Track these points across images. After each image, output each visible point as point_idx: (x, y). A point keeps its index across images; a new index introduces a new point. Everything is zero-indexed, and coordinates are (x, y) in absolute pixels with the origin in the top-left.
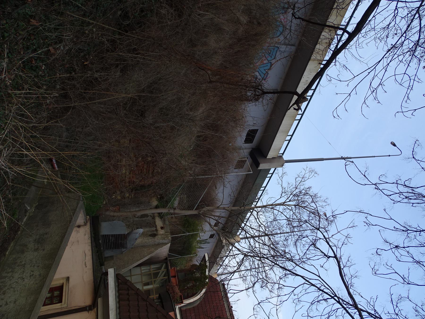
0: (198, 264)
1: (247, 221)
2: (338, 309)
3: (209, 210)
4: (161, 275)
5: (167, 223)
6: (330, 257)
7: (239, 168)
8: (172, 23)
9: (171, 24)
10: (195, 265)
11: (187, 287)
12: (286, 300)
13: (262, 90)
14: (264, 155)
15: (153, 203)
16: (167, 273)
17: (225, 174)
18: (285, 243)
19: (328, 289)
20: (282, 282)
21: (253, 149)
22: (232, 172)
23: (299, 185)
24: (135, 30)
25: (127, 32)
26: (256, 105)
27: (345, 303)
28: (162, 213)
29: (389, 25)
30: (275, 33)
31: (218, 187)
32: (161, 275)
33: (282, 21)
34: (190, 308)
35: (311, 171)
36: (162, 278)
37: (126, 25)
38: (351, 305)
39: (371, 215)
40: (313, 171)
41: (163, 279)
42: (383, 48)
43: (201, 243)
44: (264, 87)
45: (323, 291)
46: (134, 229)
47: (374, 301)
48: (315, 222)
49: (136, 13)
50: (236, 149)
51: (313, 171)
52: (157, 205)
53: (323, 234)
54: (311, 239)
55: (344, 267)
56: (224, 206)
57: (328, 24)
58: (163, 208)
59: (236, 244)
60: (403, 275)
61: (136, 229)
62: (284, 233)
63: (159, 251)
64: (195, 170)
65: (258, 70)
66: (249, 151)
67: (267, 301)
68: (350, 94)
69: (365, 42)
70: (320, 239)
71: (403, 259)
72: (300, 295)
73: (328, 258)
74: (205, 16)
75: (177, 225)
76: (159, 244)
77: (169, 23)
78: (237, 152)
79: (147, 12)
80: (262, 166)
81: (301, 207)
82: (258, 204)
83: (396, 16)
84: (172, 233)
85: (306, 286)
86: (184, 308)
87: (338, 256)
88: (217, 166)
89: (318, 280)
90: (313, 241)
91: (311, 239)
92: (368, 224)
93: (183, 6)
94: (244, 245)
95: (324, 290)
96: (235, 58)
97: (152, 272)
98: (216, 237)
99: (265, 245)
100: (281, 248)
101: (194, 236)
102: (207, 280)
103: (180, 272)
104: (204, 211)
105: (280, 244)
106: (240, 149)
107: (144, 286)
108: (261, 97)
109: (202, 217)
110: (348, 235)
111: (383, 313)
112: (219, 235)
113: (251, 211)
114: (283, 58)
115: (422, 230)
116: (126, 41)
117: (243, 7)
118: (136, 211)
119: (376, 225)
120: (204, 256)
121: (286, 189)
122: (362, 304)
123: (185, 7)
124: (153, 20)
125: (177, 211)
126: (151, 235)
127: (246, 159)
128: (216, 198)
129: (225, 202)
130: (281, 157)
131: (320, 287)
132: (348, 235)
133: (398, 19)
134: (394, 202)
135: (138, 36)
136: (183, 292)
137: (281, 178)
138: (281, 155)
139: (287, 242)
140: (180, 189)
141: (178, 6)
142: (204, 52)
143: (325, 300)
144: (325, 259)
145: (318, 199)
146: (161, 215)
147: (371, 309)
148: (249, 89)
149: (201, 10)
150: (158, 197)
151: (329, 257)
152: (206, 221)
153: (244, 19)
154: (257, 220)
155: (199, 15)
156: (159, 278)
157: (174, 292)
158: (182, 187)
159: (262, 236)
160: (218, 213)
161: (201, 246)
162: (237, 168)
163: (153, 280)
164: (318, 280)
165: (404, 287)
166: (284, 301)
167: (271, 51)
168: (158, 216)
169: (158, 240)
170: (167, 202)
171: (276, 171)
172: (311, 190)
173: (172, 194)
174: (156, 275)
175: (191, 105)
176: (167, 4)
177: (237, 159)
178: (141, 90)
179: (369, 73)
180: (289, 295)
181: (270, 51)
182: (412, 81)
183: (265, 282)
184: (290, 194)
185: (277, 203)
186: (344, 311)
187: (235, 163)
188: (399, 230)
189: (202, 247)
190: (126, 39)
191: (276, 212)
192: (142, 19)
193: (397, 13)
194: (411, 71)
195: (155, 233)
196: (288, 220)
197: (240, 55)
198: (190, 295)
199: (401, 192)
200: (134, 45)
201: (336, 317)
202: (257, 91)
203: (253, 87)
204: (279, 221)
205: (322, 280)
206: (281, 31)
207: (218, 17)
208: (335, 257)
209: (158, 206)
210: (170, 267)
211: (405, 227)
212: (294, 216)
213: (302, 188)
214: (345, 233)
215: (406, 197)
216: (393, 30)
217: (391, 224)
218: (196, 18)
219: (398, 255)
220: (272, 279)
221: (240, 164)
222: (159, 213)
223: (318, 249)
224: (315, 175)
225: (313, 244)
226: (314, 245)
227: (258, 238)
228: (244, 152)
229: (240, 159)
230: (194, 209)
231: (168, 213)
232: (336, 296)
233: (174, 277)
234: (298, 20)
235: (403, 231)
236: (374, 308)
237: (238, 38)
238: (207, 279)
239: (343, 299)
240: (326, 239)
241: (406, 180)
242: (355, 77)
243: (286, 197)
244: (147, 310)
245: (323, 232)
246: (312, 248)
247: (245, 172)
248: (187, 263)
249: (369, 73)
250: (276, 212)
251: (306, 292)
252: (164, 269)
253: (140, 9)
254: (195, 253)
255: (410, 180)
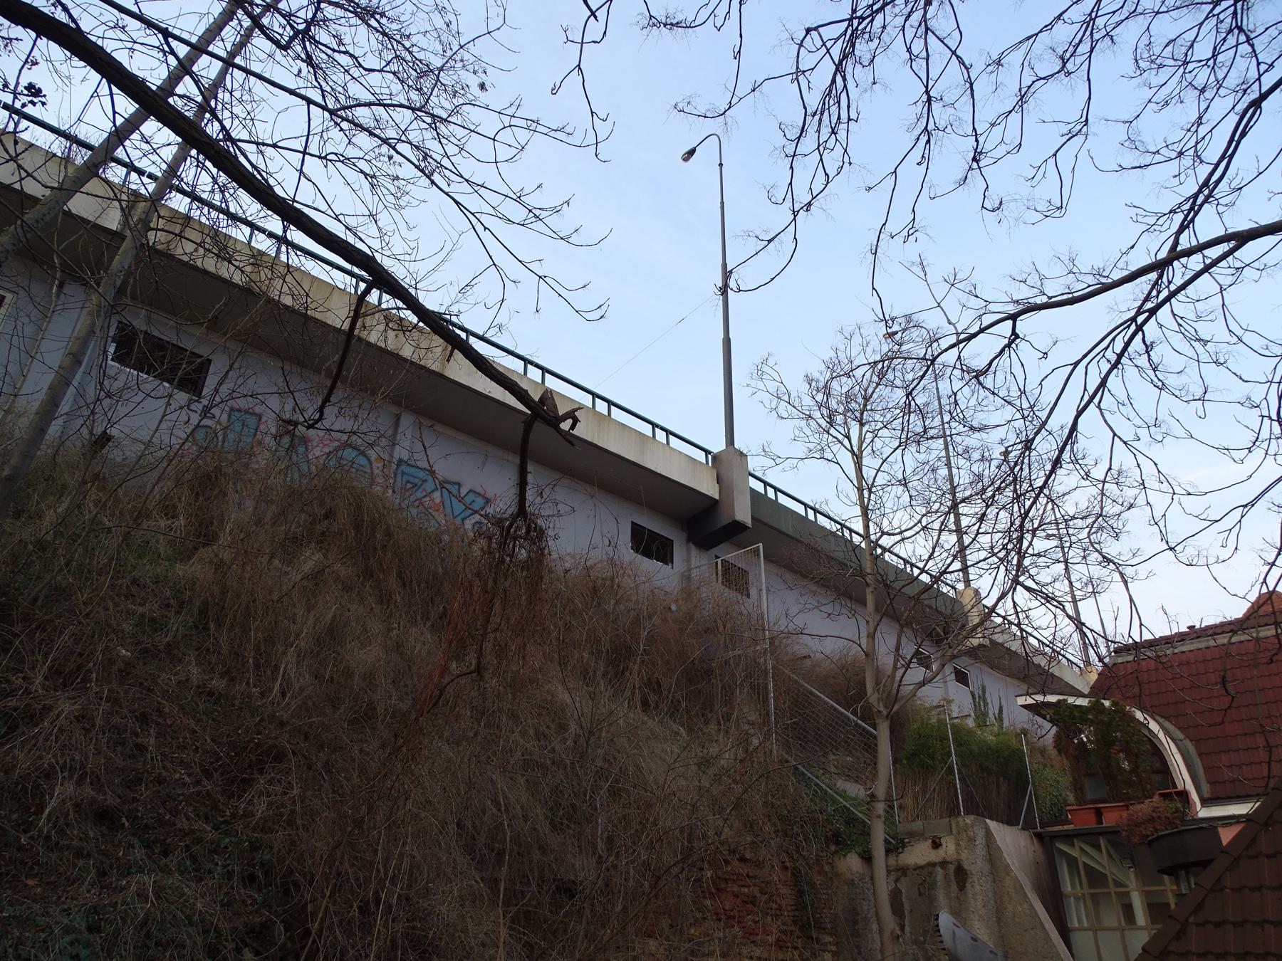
0: (1054, 729)
1: (912, 565)
2: (1174, 315)
3: (877, 684)
4: (1099, 863)
5: (918, 825)
6: (1014, 332)
7: (747, 583)
8: (297, 784)
9: (301, 787)
10: (1058, 738)
11: (1130, 772)
12: (1156, 464)
13: (514, 517)
14: (708, 507)
15: (854, 869)
16: (1090, 837)
17: (764, 630)
18: (976, 456)
19: (1114, 339)
20: (1098, 473)
21: (688, 540)
22: (760, 606)
23: (800, 409)
24: (306, 904)
25: (308, 933)
26: (556, 538)
27: (1154, 293)
28: (886, 841)
29: (366, 175)
30: (357, 470)
31: (804, 652)
32: (1099, 863)
33: (327, 450)
34: (1204, 768)
35: (759, 373)
36: (1104, 859)
37: (289, 934)
38: (1160, 277)
39: (885, 224)
40: (759, 367)
41: (1109, 855)
42: (420, 187)
43: (985, 715)
44: (504, 513)
45: (1120, 356)
46: (941, 946)
47: (1145, 213)
48: (911, 370)
49: (256, 900)
50: (689, 590)
51: (759, 367)
52: (859, 855)
53: (946, 350)
54: (961, 384)
55: (1044, 294)
56: (864, 633)
57: (346, 326)
58: (869, 835)
59: (989, 602)
60: (1063, 136)
61: (940, 936)
62: (948, 457)
63: (1015, 861)
64: (749, 723)
65: (459, 519)
66: (694, 551)
67: (1161, 524)
68: (540, 277)
69: (405, 233)
70: (959, 357)
71: (1012, 135)
72: (1139, 422)
73: (1017, 336)
74: (289, 678)
75: (925, 792)
76: (991, 860)
77: (295, 792)
78: (698, 588)
79: (255, 862)
80: (743, 513)
81: (865, 405)
82: (856, 530)
83: (343, 156)
84: (953, 812)
85: (1107, 401)
86: (1206, 788)
87: (1012, 309)
88: (740, 652)
89: (1086, 368)
90: (967, 377)
91: (961, 384)
92: (911, 230)
93: (252, 745)
94: (988, 584)
95: (1118, 352)
96: (419, 586)
97: (1087, 890)
98: (962, 663)
99: (984, 515)
100: (990, 471)
101: (962, 737)
102: (1107, 703)
103: (1082, 793)
104: (879, 699)
105: (981, 469)
106: (689, 578)
107: (1135, 924)
108: (533, 522)
109: (899, 709)
110: (945, 280)
111: (1178, 189)
112: (961, 654)
113: (879, 551)
114: (427, 456)
115: (925, 98)
116: (335, 937)
117: (276, 562)
118: (881, 931)
119: (913, 211)
120: (1024, 706)
121: (811, 446)
122: (1154, 247)
123: (255, 738)
124: (282, 843)
125: (881, 791)
126: (962, 884)
127: (719, 561)
128: (840, 659)
129: (850, 632)
130: (714, 458)
131: (1109, 361)
132: (945, 280)
133: (351, 152)
134: (846, 165)
135: (323, 897)
136: (1149, 786)
137: (778, 461)
138: (710, 456)
139: (975, 449)
140: (809, 775)
141: (251, 761)
142: (394, 682)
143: (1148, 348)
144: (1022, 346)
145: (842, 356)
146: (895, 846)
147: (1169, 221)
148: (508, 555)
149: (271, 690)
150: (836, 852)
151: (1015, 335)
152: (915, 695)
153: (311, 559)
154: (907, 534)
155: (284, 694)
156: (1104, 867)
157: (1151, 820)
158: (804, 767)
159: (957, 522)
160: (885, 657)
161: (994, 714)
162: (748, 590)
163: (1113, 889)
164: (1086, 368)
165: (1096, 135)
166: (1159, 471)
167: (408, 482)
168: (897, 856)
169: (975, 863)
170: (851, 821)
171: (759, 474)
172: (816, 375)
173: (826, 801)
174: (1095, 878)
175: (548, 727)
176: (240, 797)
177: (719, 587)
178: (489, 892)
179: (485, 228)
180: (1139, 456)
181: (409, 486)
182: (514, 121)
183: (1099, 520)
184: (826, 436)
185: (853, 475)
186: (1179, 296)
187: (730, 594)
188: (927, 152)
189: (997, 712)
190: (328, 937)
191: (881, 479)
192: (275, 879)
193: (336, 154)
194: (489, 124)
195: (952, 868)
196: (903, 445)
197: (411, 572)
198: (1158, 765)
199: (819, 146)
200: (349, 912)
201: (1199, 318)
202: (515, 531)
203: (502, 545)
204: (909, 471)
205: (1085, 356)
206: (355, 453)
207: (298, 636)
208: (1014, 317)
209: (864, 852)
210: (1066, 827)
211: (918, 139)
212: (894, 426)
213: (808, 401)
214: (940, 289)
215: (834, 132)
216: (379, 165)
217: (911, 173)
218: (293, 703)
219: (1001, 150)
220: (1092, 499)
221: (735, 578)
222: (888, 852)
223: (990, 364)
224: (771, 362)
225: (977, 377)
226: (978, 375)
227: (965, 536)
228: (699, 567)
229: (720, 578)
230: (874, 732)
231: (887, 819)
232: (1134, 319)
233: (1099, 813)
234: (327, 411)
235: (928, 141)
236: (1165, 215)
237: (362, 578)
238: (1103, 704)
239: (1142, 297)
240: (959, 342)
241: (785, 135)
242: (494, 264)
243: (836, 447)
244: (1217, 925)
245: (940, 351)
246: (988, 381)
247: (760, 566)
248: (1052, 767)
249: (485, 228)
250: (881, 479)
251: (1126, 401)
252: (1073, 845)
253: (244, 885)
254: (1018, 735)
255: (782, 127)
